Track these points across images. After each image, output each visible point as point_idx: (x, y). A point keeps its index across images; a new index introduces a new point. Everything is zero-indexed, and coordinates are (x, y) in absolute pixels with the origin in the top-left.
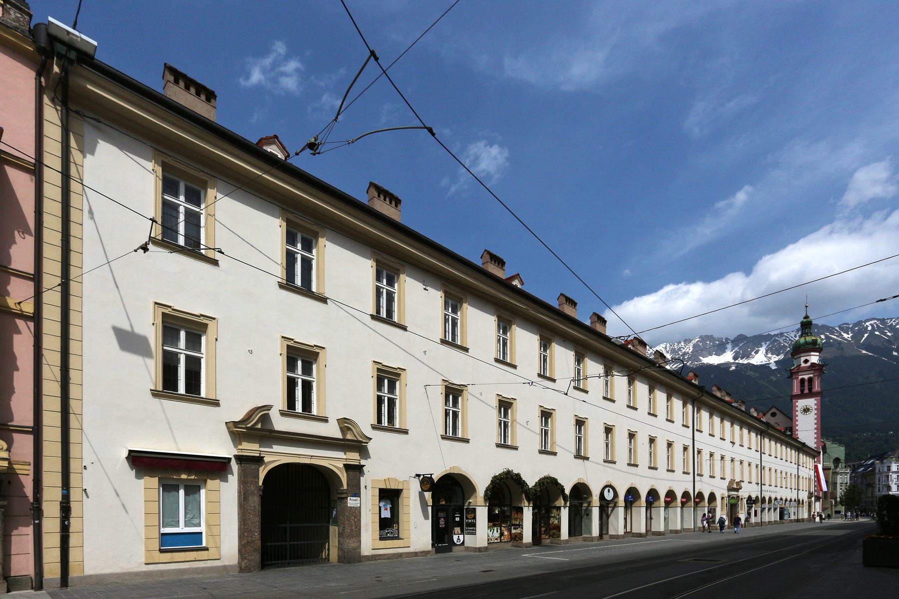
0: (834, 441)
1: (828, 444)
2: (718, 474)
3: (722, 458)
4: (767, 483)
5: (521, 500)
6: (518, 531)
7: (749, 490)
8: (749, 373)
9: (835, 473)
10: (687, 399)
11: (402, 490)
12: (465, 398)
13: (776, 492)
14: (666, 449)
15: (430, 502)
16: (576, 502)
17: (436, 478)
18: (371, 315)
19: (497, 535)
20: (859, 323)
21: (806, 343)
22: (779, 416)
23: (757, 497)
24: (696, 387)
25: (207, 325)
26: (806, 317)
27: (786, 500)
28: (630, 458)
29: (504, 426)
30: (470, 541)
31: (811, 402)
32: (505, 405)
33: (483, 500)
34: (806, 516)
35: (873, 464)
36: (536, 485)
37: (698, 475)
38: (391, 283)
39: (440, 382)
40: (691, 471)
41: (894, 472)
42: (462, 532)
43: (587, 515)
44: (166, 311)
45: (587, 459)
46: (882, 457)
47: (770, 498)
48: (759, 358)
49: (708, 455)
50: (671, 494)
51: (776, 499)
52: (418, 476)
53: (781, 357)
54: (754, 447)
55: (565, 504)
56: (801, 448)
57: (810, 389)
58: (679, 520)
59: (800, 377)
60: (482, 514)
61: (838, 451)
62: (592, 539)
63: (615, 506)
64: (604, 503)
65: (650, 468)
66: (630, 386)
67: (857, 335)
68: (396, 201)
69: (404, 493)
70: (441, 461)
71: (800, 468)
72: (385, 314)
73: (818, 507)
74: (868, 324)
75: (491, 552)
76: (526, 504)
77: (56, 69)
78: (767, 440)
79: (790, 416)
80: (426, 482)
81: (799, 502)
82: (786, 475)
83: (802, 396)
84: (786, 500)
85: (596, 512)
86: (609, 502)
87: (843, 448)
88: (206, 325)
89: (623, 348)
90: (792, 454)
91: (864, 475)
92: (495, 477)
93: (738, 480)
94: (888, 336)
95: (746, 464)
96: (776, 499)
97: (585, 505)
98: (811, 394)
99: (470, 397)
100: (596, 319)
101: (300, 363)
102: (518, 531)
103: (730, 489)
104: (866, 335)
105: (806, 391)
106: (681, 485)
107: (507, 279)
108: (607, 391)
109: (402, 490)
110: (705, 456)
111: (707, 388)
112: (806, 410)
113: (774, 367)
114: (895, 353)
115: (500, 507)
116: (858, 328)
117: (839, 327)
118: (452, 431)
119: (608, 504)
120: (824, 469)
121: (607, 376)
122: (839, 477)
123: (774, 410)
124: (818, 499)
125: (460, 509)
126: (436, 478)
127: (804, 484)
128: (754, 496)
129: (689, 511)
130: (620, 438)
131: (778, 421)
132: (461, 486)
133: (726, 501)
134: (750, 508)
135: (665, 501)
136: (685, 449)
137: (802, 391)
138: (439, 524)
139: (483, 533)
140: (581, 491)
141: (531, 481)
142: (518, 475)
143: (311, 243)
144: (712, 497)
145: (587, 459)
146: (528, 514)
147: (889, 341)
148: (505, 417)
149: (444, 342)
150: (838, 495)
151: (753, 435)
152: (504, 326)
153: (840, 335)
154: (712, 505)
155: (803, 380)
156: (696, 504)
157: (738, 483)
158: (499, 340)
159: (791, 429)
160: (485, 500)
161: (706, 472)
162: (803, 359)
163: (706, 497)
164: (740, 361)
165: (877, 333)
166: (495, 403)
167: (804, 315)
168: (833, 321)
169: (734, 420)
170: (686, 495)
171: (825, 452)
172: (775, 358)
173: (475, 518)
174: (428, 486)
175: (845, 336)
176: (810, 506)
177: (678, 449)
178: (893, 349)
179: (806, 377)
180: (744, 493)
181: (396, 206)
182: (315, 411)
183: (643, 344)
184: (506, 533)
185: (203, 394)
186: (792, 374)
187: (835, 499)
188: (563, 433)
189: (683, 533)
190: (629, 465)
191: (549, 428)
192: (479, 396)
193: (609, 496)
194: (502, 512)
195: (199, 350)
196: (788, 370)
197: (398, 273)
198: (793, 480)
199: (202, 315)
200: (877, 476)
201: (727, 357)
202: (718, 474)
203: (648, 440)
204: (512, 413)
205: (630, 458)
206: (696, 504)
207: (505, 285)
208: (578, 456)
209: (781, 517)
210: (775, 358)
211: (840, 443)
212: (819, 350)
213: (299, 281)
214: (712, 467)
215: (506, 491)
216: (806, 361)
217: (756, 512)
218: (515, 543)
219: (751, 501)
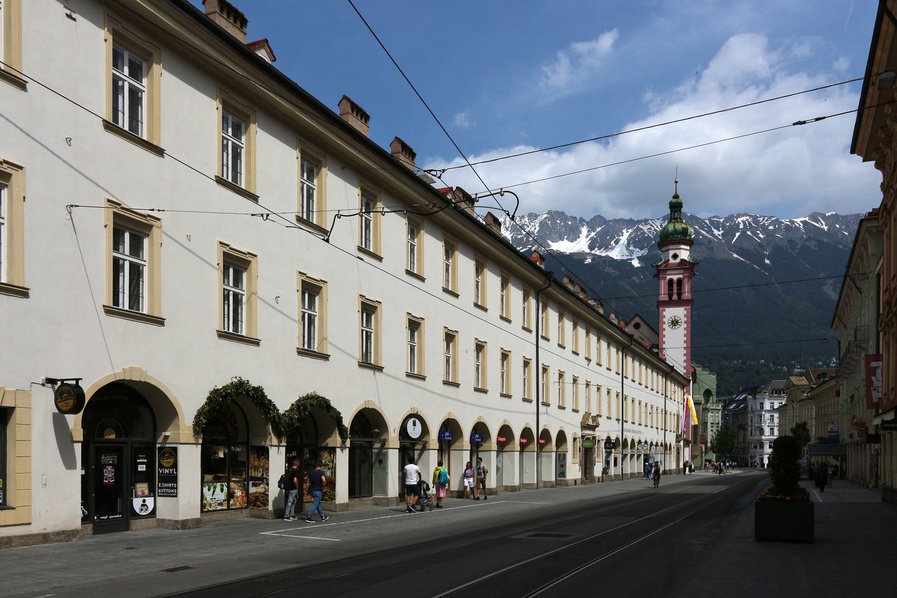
0: (704, 368)
1: (699, 370)
2: (569, 405)
3: (575, 381)
4: (630, 420)
5: (265, 436)
6: (260, 489)
7: (607, 429)
8: (608, 270)
9: (706, 410)
10: (530, 289)
11: (12, 409)
12: (157, 241)
13: (639, 432)
14: (500, 362)
15: (78, 434)
16: (361, 440)
17: (89, 388)
18: (104, 121)
19: (221, 496)
20: (730, 218)
21: (675, 231)
22: (644, 328)
23: (617, 439)
24: (545, 279)
26: (676, 197)
27: (652, 444)
28: (448, 373)
29: (234, 303)
30: (166, 508)
31: (680, 312)
32: (235, 264)
33: (191, 432)
34: (674, 467)
35: (745, 399)
36: (291, 409)
37: (544, 404)
38: (136, 73)
39: (103, 203)
40: (534, 398)
41: (766, 411)
42: (152, 492)
43: (381, 462)
44: (116, 210)
45: (380, 369)
46: (754, 391)
47: (633, 441)
51: (640, 442)
52: (51, 381)
53: (645, 252)
54: (614, 368)
55: (344, 442)
56: (668, 373)
59: (668, 277)
60: (189, 460)
61: (709, 380)
62: (388, 501)
63: (424, 448)
64: (407, 443)
65: (476, 390)
66: (447, 258)
67: (729, 232)
68: (365, 117)
69: (18, 416)
72: (127, 124)
73: (686, 454)
74: (740, 220)
75: (207, 528)
76: (275, 441)
78: (629, 359)
79: (656, 330)
80: (68, 394)
81: (666, 447)
82: (650, 410)
83: (670, 303)
84: (652, 444)
85: (393, 457)
86: (414, 442)
87: (714, 377)
88: (9, 176)
90: (657, 380)
92: (215, 392)
93: (594, 414)
94: (760, 238)
95: (604, 391)
96: (640, 442)
97: (377, 445)
98: (680, 303)
99: (165, 240)
100: (400, 149)
101: (127, 236)
102: (260, 489)
103: (585, 427)
104: (738, 234)
105: (675, 297)
107: (250, 45)
108: (412, 262)
109: (12, 409)
110: (553, 376)
111: (555, 276)
112: (675, 323)
113: (636, 263)
114: (767, 261)
115: (227, 445)
117: (710, 220)
118: (128, 298)
119: (414, 445)
120: (695, 404)
121: (368, 212)
122: (710, 414)
123: (637, 320)
124: (687, 443)
125: (149, 450)
126: (89, 388)
127: (671, 423)
128: (613, 438)
129: (531, 457)
130: (432, 339)
131: (643, 334)
132: (147, 405)
134: (609, 454)
135: (498, 443)
136: (526, 364)
137: (670, 296)
138: (102, 476)
139: (190, 492)
140: (369, 422)
141: (283, 402)
142: (259, 390)
143: (141, 67)
145: (380, 369)
146: (277, 462)
147: (760, 245)
149: (220, 181)
150: (709, 440)
151: (613, 350)
152: (310, 168)
153: (710, 232)
154: (561, 449)
155: (671, 282)
156: (541, 447)
157: (595, 419)
158: (302, 188)
160: (196, 433)
161: (554, 400)
162: (671, 253)
163: (554, 436)
164: (596, 252)
165: (749, 233)
166: (216, 257)
167: (673, 194)
169: (590, 327)
172: (638, 253)
173: (175, 466)
174: (71, 402)
175: (716, 232)
176: (678, 453)
177: (516, 362)
178: (764, 256)
179: (675, 278)
180: (601, 433)
181: (241, 27)
183: (470, 200)
184: (238, 493)
186: (659, 271)
188: (340, 324)
189: (522, 492)
190: (446, 383)
192: (185, 241)
193: (414, 431)
194: (232, 456)
196: (655, 268)
197: (149, 59)
198: (660, 415)
199: (249, 253)
200: (750, 415)
201: (580, 245)
202: (569, 405)
203: (473, 347)
204: (151, 244)
205: (448, 373)
206: (541, 447)
207: (246, 53)
208: (365, 363)
211: (711, 371)
212: (690, 243)
213: (127, 124)
214: (561, 393)
215: (234, 417)
217: (616, 459)
218: (256, 511)
219: (610, 444)
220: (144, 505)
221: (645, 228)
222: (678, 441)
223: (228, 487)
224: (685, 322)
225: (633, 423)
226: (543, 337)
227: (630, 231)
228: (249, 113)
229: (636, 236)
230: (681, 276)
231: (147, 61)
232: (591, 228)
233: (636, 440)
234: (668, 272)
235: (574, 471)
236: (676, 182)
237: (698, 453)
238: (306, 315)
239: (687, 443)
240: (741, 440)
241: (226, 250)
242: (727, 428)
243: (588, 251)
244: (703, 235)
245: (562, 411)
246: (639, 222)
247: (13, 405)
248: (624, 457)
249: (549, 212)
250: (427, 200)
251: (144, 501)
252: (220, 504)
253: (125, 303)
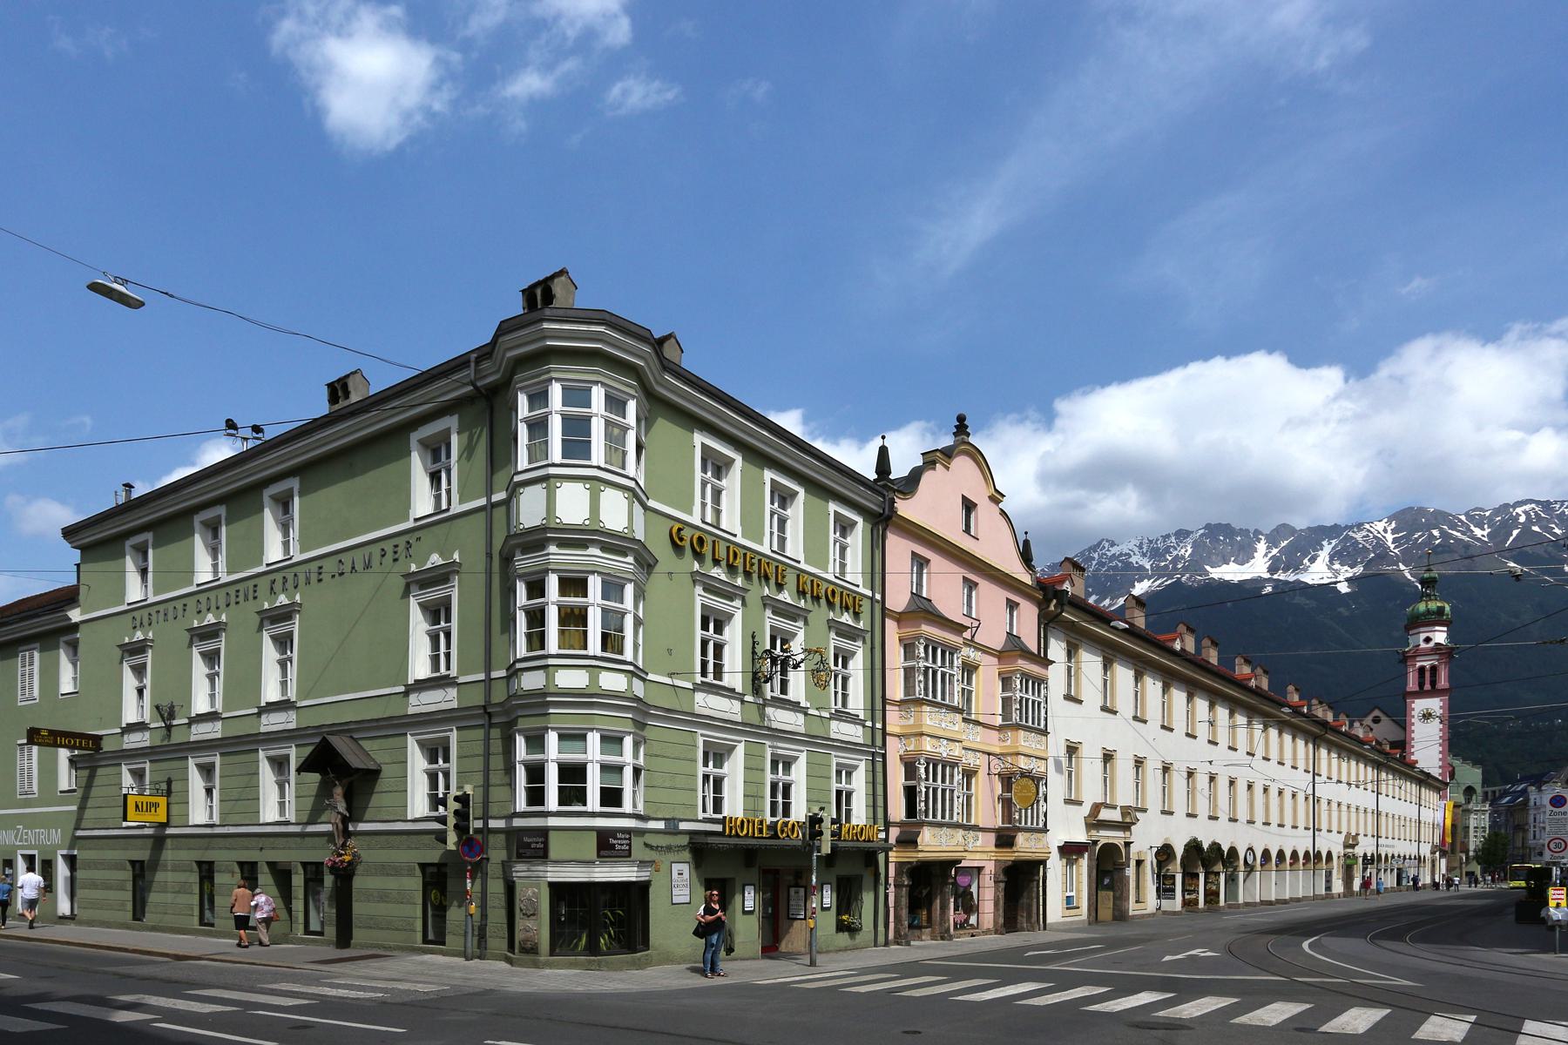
0: (1465, 759)
1: (1457, 763)
2: (1335, 829)
7: (1365, 847)
8: (1299, 600)
21: (1428, 612)
31: (1435, 704)
34: (1428, 881)
35: (1524, 791)
48: (1318, 572)
50: (1294, 854)
53: (1359, 570)
56: (1424, 780)
57: (1433, 683)
58: (1296, 885)
61: (1472, 775)
67: (1500, 532)
74: (1519, 510)
77: (1052, 608)
79: (1401, 721)
83: (1421, 693)
91: (1511, 810)
94: (1555, 535)
98: (1434, 692)
103: (1346, 846)
104: (1515, 532)
105: (1427, 687)
106: (1303, 843)
112: (1427, 716)
113: (1343, 588)
116: (1503, 518)
117: (1467, 514)
127: (1426, 833)
131: (1384, 730)
137: (1421, 685)
150: (1472, 847)
155: (1422, 669)
157: (1126, 811)
159: (1402, 745)
162: (1423, 636)
164: (1281, 576)
165: (1536, 528)
168: (1458, 509)
172: (1346, 572)
175: (1478, 532)
177: (1301, 797)
180: (1358, 851)
187: (1467, 852)
200: (1532, 812)
201: (1257, 567)
202: (1335, 829)
209: (1399, 883)
210: (1346, 572)
216: (1428, 640)
219: (1368, 861)
221: (1359, 536)
222: (1433, 853)
227: (1334, 542)
229: (1344, 548)
232: (1272, 541)
235: (1338, 887)
237: (1457, 864)
238: (711, 645)
240: (1519, 844)
242: (1496, 835)
243: (1267, 576)
244: (1456, 539)
246: (1350, 528)
248: (1379, 871)
249: (1208, 526)
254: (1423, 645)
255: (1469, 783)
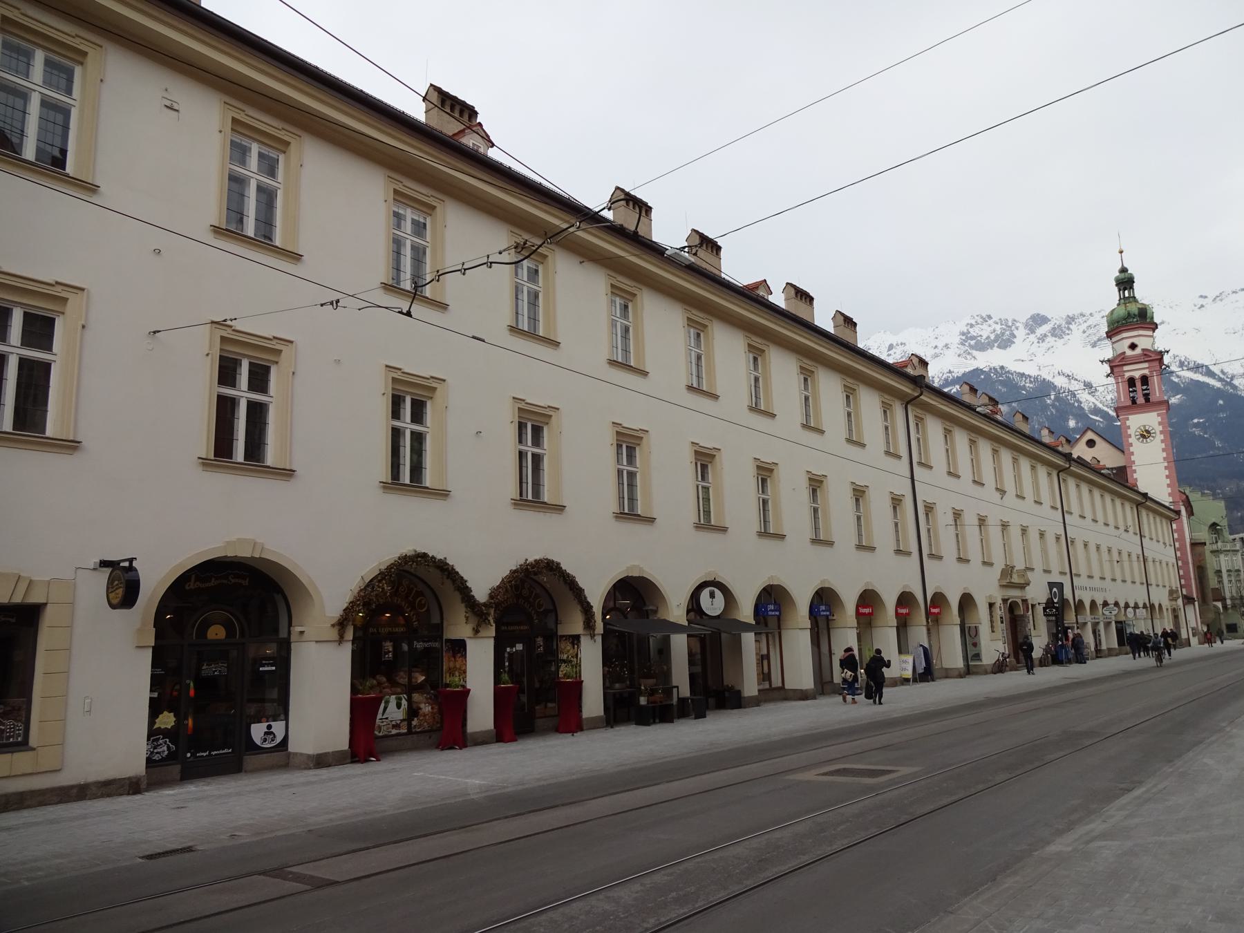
0: (1201, 489)
2: (974, 554)
4: (1083, 571)
13: (1103, 590)
25: (550, 416)
27: (1127, 606)
31: (1151, 419)
37: (931, 556)
44: (395, 376)
47: (1093, 603)
49: (1038, 536)
51: (1105, 604)
59: (1127, 375)
69: (48, 619)
70: (192, 520)
71: (1146, 541)
72: (530, 329)
84: (1127, 606)
89: (895, 370)
93: (1020, 565)
96: (1105, 604)
110: (943, 518)
112: (1145, 435)
123: (1090, 435)
124: (1188, 600)
130: (838, 500)
133: (998, 613)
137: (1134, 401)
144: (967, 601)
148: (703, 478)
161: (948, 547)
163: (954, 602)
170: (905, 599)
171: (1191, 513)
177: (1050, 539)
179: (1137, 375)
182: (270, 460)
185: (50, 431)
187: (1223, 600)
188: (668, 483)
191: (820, 505)
193: (713, 605)
195: (48, 347)
198: (1135, 564)
202: (974, 554)
208: (764, 534)
216: (1133, 346)
220: (269, 732)
223: (409, 700)
224: (1161, 432)
225: (1090, 577)
226: (920, 463)
228: (434, 204)
230: (1146, 372)
231: (82, 64)
233: (1099, 602)
234: (1126, 368)
236: (1121, 252)
239: (1188, 600)
241: (697, 448)
245: (988, 568)
247: (43, 601)
250: (566, 222)
251: (269, 727)
252: (394, 727)
253: (406, 477)
254: (1129, 353)
255: (1213, 520)
